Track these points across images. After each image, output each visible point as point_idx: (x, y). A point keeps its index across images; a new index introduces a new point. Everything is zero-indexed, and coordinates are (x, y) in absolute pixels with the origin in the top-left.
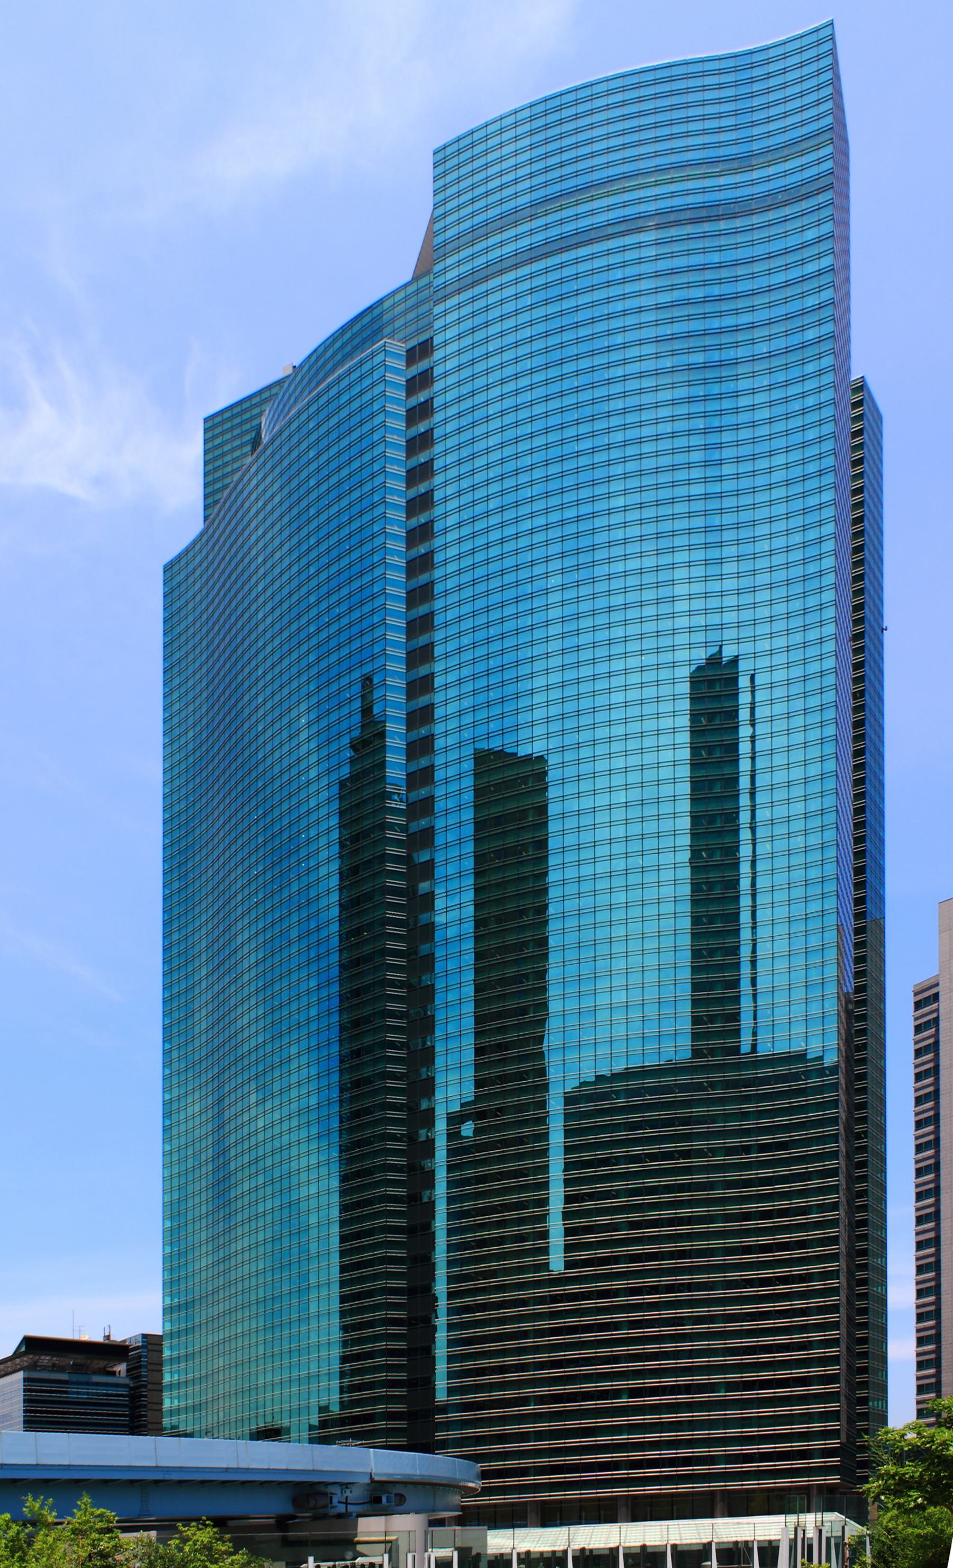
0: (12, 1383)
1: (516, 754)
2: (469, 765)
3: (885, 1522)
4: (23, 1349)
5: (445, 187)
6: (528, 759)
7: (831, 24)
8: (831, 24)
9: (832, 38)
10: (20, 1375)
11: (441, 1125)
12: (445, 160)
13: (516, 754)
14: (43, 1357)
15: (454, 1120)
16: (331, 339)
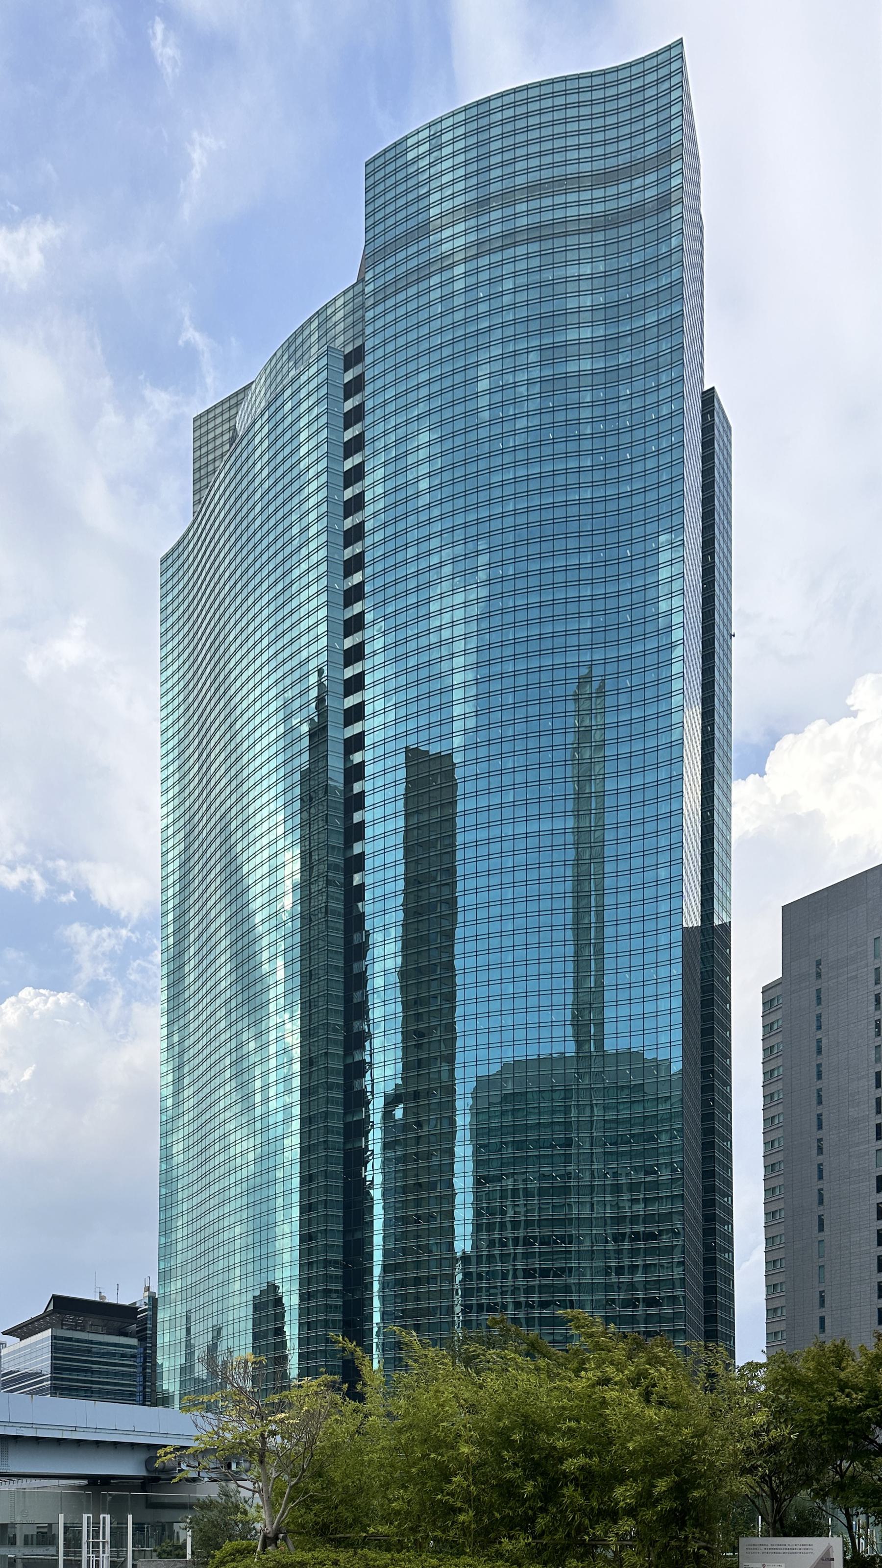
0: (42, 1341)
1: (428, 751)
2: (401, 758)
3: (595, 1199)
4: (51, 1307)
5: (375, 211)
6: (439, 757)
7: (680, 42)
8: (680, 42)
9: (681, 56)
10: (48, 1333)
11: (377, 1104)
12: (375, 172)
13: (428, 751)
14: (68, 1316)
15: (391, 1101)
16: (287, 344)
